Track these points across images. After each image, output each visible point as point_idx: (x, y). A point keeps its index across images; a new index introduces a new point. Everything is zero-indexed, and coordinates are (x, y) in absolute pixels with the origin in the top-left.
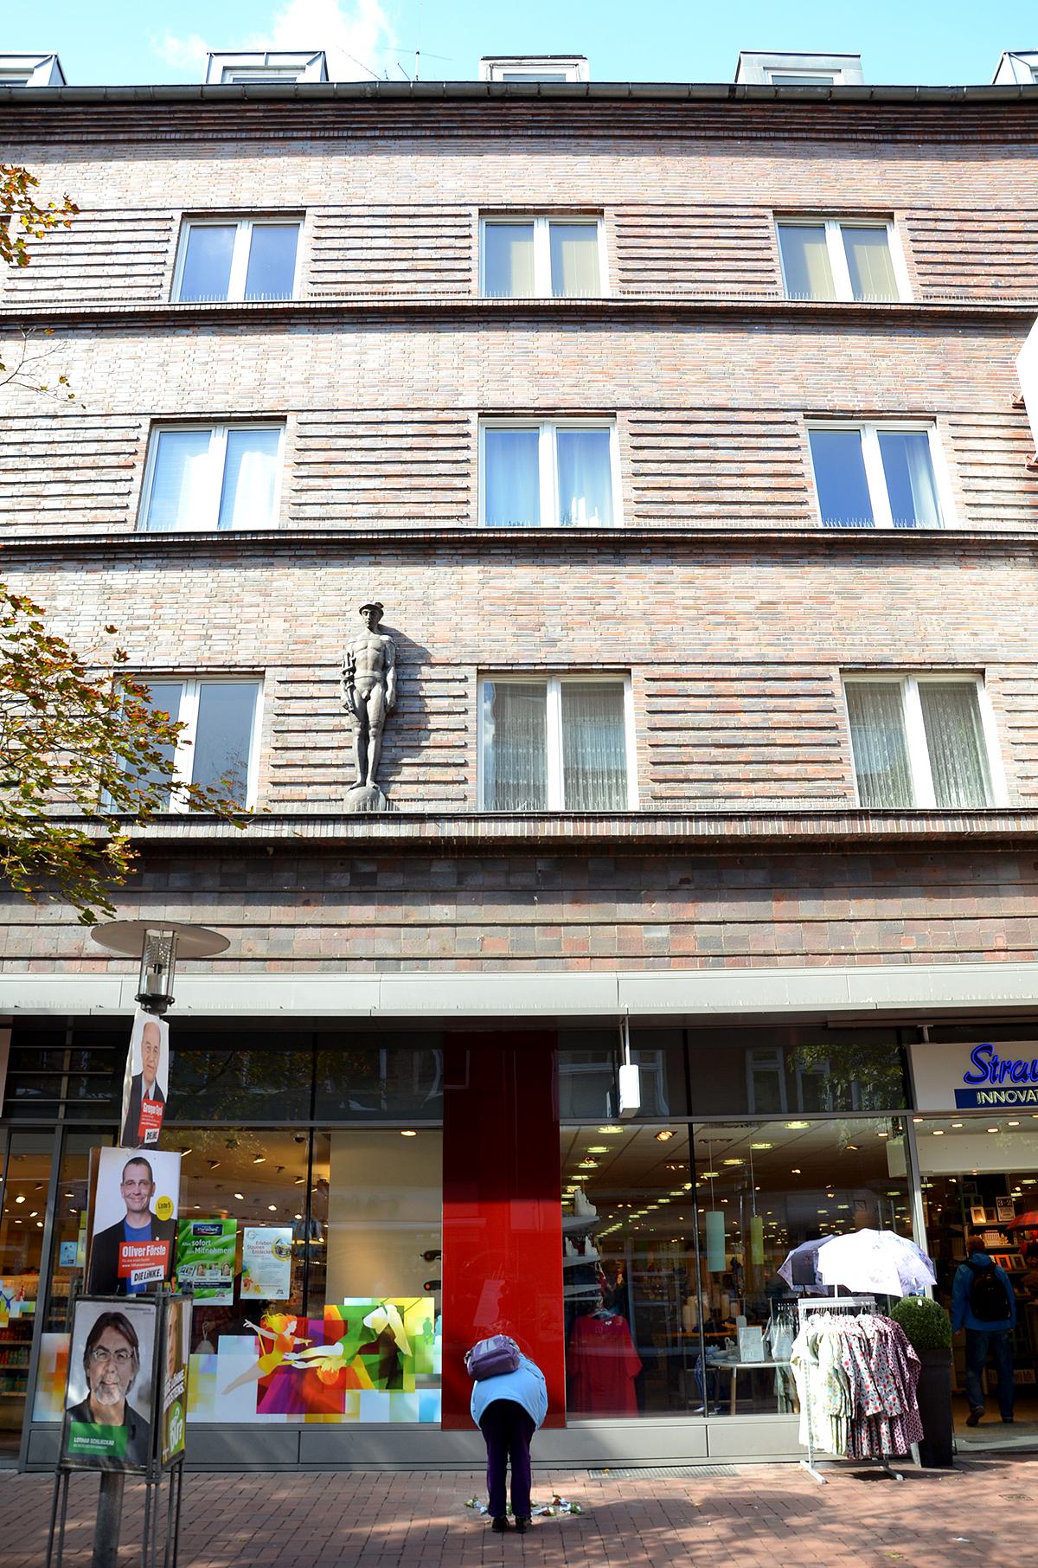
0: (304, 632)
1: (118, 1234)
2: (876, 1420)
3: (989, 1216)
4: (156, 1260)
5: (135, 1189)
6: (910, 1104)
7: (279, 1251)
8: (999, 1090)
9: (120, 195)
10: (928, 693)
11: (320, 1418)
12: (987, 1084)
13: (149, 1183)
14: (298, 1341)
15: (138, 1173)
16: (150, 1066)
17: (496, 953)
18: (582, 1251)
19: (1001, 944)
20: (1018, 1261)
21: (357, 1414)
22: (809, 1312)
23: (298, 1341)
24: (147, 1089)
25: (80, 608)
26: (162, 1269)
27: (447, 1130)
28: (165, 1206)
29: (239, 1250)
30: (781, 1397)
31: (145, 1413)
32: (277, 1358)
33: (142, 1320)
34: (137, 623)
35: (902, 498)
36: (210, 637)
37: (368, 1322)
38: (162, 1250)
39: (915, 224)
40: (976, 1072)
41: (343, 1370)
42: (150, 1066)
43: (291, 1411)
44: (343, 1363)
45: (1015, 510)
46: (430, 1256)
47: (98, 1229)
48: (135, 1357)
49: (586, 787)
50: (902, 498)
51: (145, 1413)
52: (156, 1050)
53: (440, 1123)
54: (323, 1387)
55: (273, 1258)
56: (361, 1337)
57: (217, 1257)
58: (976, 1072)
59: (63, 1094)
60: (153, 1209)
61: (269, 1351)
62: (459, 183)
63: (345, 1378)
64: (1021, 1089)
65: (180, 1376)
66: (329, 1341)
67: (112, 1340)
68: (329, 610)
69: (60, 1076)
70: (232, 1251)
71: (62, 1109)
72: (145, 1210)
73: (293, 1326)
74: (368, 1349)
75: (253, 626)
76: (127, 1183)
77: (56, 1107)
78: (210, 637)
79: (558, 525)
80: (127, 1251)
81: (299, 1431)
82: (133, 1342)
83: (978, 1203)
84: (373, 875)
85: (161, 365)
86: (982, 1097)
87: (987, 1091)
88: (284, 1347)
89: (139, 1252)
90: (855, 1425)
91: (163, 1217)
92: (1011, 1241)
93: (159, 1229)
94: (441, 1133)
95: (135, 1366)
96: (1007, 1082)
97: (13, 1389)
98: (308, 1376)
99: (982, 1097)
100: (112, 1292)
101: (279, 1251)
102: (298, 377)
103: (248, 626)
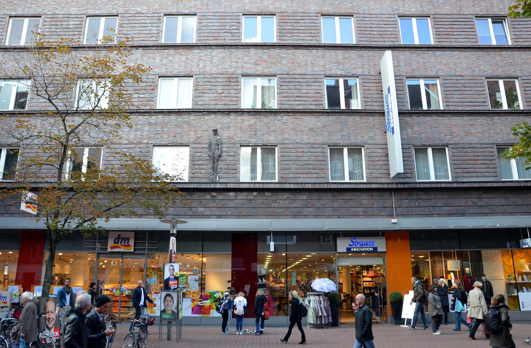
0: (198, 135)
1: (168, 279)
2: (321, 317)
3: (367, 273)
4: (175, 284)
5: (171, 271)
6: (336, 250)
7: (196, 280)
8: (356, 248)
9: (147, 8)
10: (350, 152)
11: (205, 315)
12: (354, 246)
13: (174, 270)
14: (200, 299)
15: (172, 268)
16: (173, 247)
17: (244, 214)
18: (262, 281)
19: (361, 214)
20: (373, 284)
21: (213, 315)
22: (309, 295)
23: (200, 299)
24: (173, 252)
25: (144, 128)
26: (176, 285)
27: (232, 254)
28: (177, 274)
29: (187, 280)
30: (325, 317)
31: (176, 311)
32: (196, 303)
33: (175, 295)
34: (158, 132)
35: (348, 104)
36: (176, 136)
37: (215, 295)
38: (176, 282)
39: (359, 19)
40: (352, 244)
41: (210, 306)
42: (173, 247)
43: (199, 314)
44: (210, 304)
45: (376, 103)
46: (229, 282)
47: (165, 278)
48: (173, 301)
49: (266, 173)
50: (348, 104)
51: (176, 311)
52: (174, 244)
53: (231, 253)
54: (205, 309)
55: (195, 282)
56: (214, 299)
57: (182, 282)
58: (352, 244)
59: (147, 246)
60: (174, 275)
61: (194, 301)
62: (238, 6)
63: (210, 307)
64: (362, 248)
65: (181, 305)
66: (207, 300)
67: (169, 298)
68: (205, 129)
69: (146, 242)
70: (185, 280)
71: (147, 249)
72: (173, 275)
73: (199, 296)
74: (215, 301)
75: (186, 133)
76: (170, 270)
77: (145, 249)
78: (176, 136)
79: (275, 41)
80: (170, 282)
81: (201, 318)
82: (173, 299)
83: (365, 270)
84: (216, 196)
85: (160, 61)
86: (352, 249)
87: (354, 248)
88: (197, 301)
89: (172, 282)
90: (317, 318)
91: (176, 276)
92: (372, 279)
93: (176, 278)
94: (231, 255)
95: (173, 303)
96: (359, 246)
97: (129, 311)
98: (202, 307)
99: (352, 249)
100: (168, 290)
101: (196, 280)
102: (195, 64)
103: (185, 133)
